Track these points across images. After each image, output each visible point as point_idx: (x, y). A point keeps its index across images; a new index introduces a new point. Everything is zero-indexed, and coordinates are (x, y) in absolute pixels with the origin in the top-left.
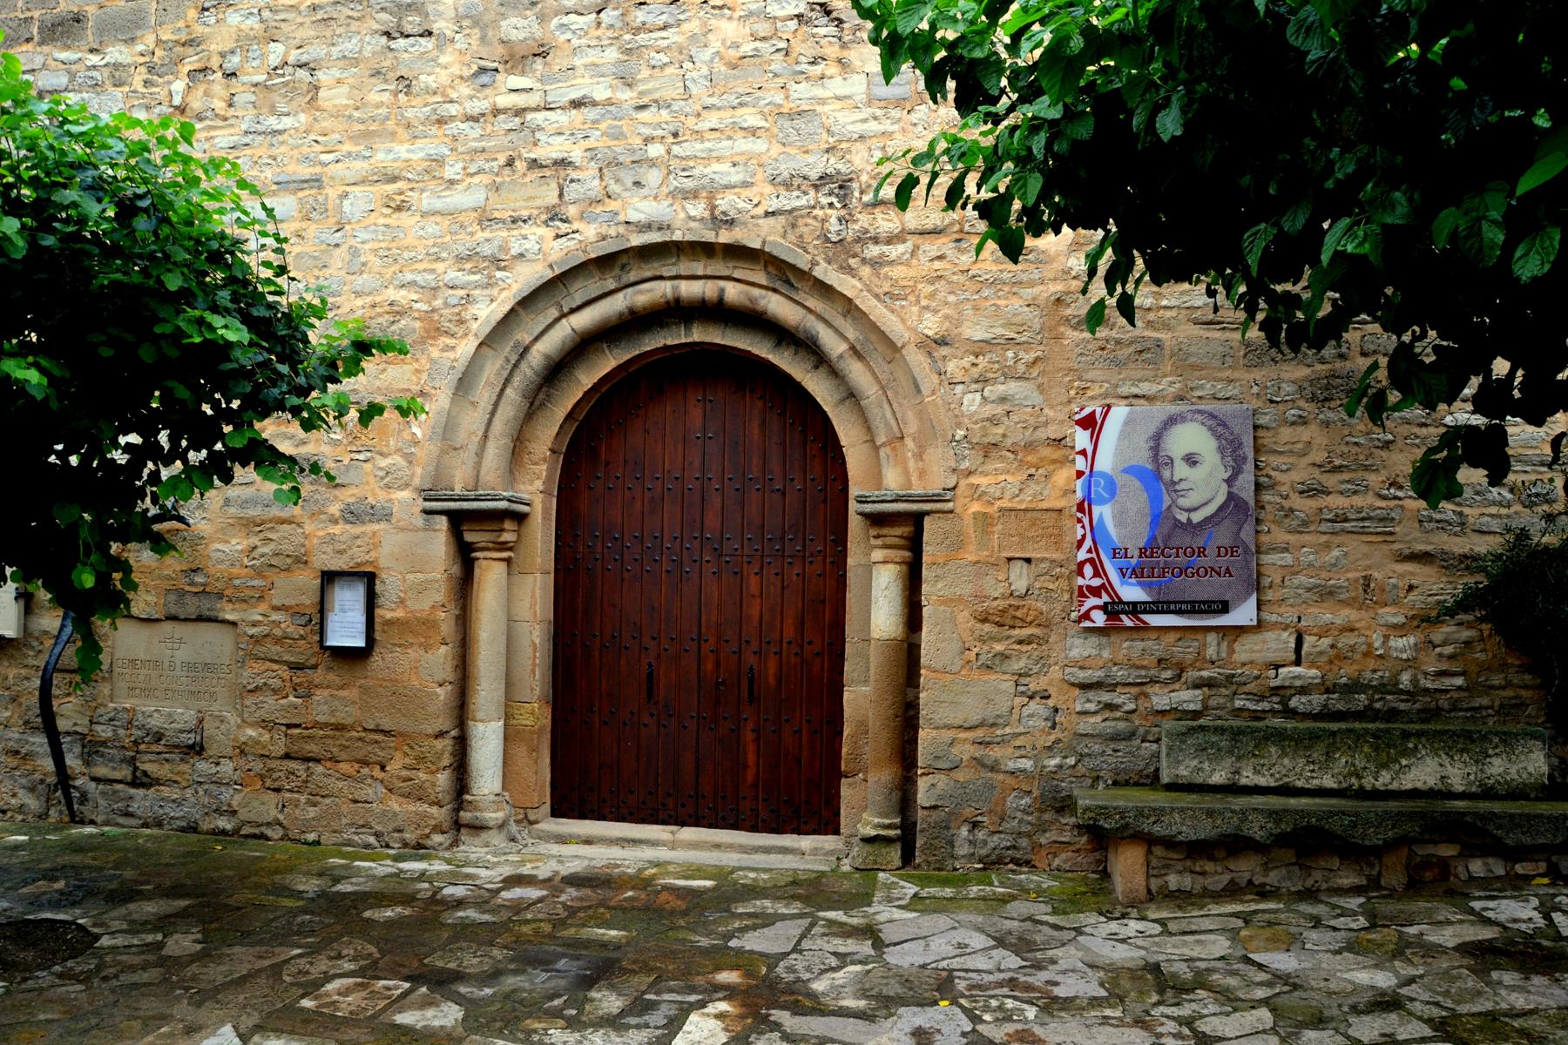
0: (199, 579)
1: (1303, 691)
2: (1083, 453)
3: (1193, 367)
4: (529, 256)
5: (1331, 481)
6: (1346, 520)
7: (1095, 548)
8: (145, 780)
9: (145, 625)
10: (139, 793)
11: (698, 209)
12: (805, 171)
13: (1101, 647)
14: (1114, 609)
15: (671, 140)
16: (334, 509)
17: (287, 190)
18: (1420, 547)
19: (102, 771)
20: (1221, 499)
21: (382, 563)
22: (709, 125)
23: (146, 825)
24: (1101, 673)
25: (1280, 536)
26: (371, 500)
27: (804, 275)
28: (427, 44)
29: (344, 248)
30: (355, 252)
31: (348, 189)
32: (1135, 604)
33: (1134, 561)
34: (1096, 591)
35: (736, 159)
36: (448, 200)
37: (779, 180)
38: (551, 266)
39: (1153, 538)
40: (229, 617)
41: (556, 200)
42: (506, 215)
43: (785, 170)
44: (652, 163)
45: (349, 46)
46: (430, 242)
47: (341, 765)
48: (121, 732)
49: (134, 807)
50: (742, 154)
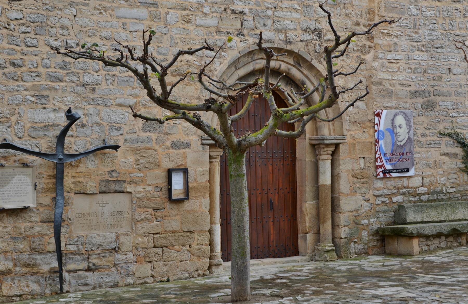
0: (115, 175)
1: (424, 194)
2: (377, 124)
3: (399, 98)
4: (233, 48)
5: (427, 132)
6: (431, 144)
7: (380, 154)
8: (93, 267)
9: (91, 196)
10: (90, 274)
12: (310, 27)
13: (126, 188)
14: (385, 172)
15: (274, 9)
16: (168, 143)
17: (144, 6)
18: (446, 151)
20: (406, 138)
21: (188, 165)
22: (285, 6)
23: (94, 288)
24: (381, 192)
26: (182, 140)
27: (305, 60)
29: (169, 35)
30: (172, 37)
31: (169, 10)
32: (389, 170)
33: (389, 157)
34: (380, 167)
35: (292, 20)
36: (205, 21)
37: (303, 29)
38: (239, 52)
39: (393, 150)
40: (129, 190)
41: (240, 27)
42: (225, 31)
43: (305, 25)
44: (268, 17)
46: (200, 38)
48: (81, 247)
49: (89, 281)
50: (294, 18)
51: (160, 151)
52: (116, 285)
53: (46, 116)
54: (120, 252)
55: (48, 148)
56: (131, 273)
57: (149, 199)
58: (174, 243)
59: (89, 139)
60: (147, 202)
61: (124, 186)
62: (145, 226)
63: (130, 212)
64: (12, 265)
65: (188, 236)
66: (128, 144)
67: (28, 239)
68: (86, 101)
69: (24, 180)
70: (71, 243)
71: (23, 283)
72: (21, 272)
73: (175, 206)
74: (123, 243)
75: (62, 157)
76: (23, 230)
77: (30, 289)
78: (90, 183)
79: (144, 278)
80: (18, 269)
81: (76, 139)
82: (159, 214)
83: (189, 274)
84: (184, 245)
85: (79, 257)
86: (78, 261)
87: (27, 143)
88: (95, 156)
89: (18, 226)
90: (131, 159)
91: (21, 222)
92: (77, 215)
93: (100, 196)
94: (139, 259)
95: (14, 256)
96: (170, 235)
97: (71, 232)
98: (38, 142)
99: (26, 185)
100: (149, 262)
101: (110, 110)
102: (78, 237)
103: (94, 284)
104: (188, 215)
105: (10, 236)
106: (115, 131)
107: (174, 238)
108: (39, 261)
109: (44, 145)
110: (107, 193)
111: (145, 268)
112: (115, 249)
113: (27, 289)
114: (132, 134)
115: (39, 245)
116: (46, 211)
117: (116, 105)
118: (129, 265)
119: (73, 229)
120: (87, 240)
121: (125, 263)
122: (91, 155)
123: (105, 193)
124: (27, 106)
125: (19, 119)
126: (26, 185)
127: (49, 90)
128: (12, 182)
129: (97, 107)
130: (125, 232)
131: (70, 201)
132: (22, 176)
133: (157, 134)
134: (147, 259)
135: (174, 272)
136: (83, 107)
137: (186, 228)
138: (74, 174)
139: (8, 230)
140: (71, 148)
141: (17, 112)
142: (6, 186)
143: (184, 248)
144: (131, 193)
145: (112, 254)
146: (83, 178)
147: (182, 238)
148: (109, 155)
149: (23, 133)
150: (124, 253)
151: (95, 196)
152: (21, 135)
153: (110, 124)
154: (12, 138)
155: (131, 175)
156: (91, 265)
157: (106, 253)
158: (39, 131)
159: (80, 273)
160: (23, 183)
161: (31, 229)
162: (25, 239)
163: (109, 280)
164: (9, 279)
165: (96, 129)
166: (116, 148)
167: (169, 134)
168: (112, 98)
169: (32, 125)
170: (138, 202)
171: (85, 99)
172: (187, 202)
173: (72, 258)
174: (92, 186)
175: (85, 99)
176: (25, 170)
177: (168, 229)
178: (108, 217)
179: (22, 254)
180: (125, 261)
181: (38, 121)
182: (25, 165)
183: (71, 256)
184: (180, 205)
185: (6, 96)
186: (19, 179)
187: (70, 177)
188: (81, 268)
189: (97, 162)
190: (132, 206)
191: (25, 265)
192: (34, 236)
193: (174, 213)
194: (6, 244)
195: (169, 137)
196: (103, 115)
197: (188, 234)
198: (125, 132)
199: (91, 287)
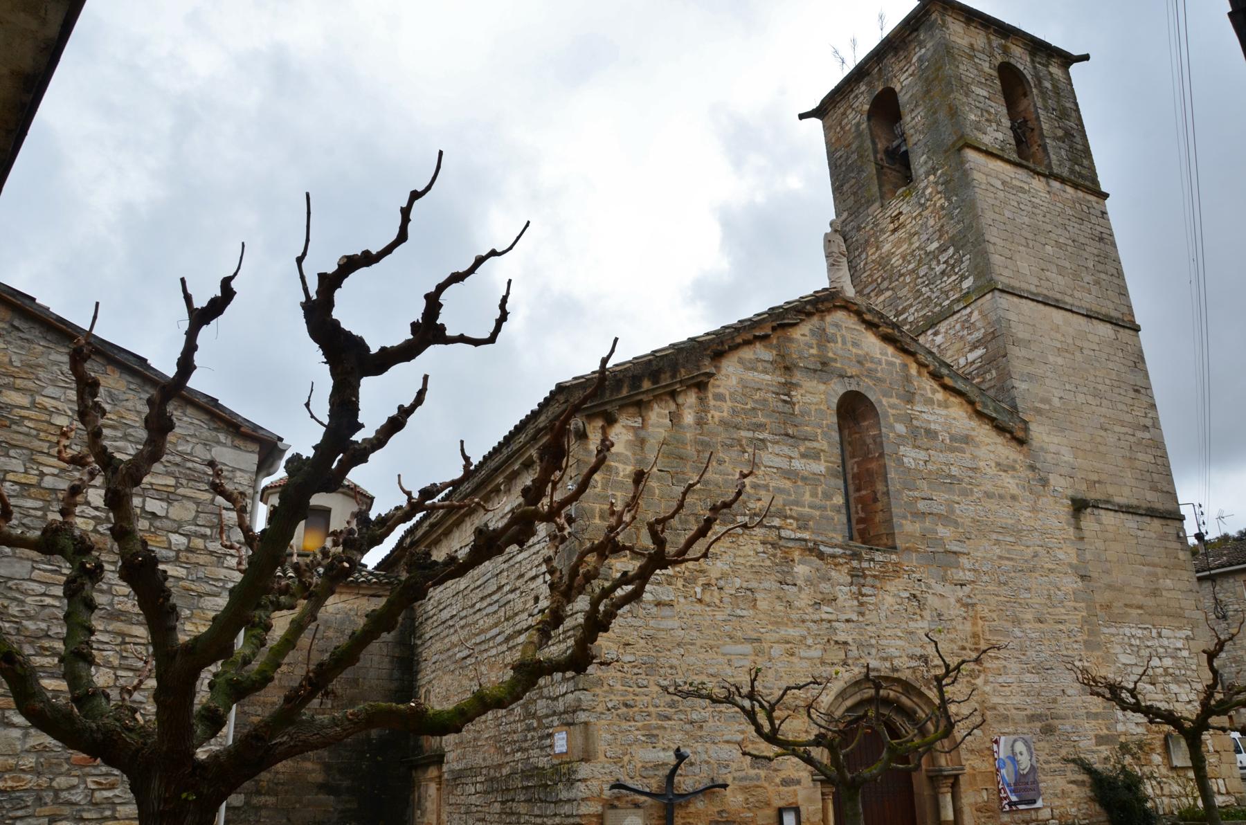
11: (888, 665)
16: (778, 780)
25: (1043, 777)
28: (795, 589)
45: (766, 585)
51: (770, 788)
90: (740, 798)
165: (705, 767)
185: (619, 736)
196: (710, 752)
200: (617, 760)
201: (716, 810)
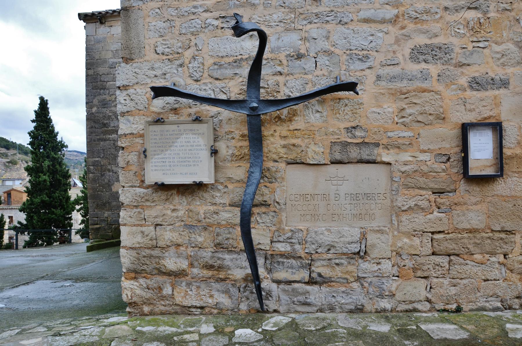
0: (358, 133)
8: (319, 279)
9: (312, 168)
10: (314, 288)
13: (380, 155)
16: (463, 81)
19: (282, 275)
21: (503, 118)
23: (321, 310)
26: (492, 74)
40: (385, 159)
47: (475, 256)
48: (297, 247)
49: (311, 299)
51: (448, 93)
52: (359, 310)
53: (238, 45)
54: (369, 258)
55: (240, 94)
56: (387, 294)
57: (424, 175)
58: (472, 249)
59: (310, 77)
60: (421, 179)
61: (376, 152)
62: (416, 219)
63: (388, 195)
64: (187, 264)
65: (501, 239)
66: (383, 83)
67: (211, 229)
68: (304, 19)
69: (194, 142)
70: (281, 239)
71: (205, 291)
72: (201, 275)
73: (476, 188)
74: (373, 246)
75: (255, 105)
76: (203, 216)
77: (215, 301)
78: (312, 147)
79: (412, 302)
80: (195, 271)
81: (288, 78)
82: (442, 200)
83: (502, 301)
84: (493, 254)
85: (294, 261)
86: (292, 267)
87: (207, 88)
88: (322, 102)
89: (195, 210)
90: (390, 107)
91: (198, 203)
92: (293, 197)
93: (333, 169)
94: (404, 272)
95: (190, 251)
96: (465, 235)
97: (280, 222)
98: (223, 85)
99: (197, 150)
100: (422, 278)
101: (348, 29)
102: (292, 231)
103: (320, 304)
104: (504, 203)
105: (183, 223)
106: (358, 62)
107: (472, 241)
108: (227, 263)
109: (235, 88)
110: (345, 163)
111: (415, 288)
112: (358, 253)
113: (210, 301)
114: (392, 67)
115: (227, 239)
116: (238, 190)
117: (358, 21)
118: (384, 281)
119: (284, 218)
120: (309, 236)
121: (378, 276)
122: (313, 101)
123: (340, 162)
124: (208, 33)
125: (196, 53)
126: (197, 150)
127: (243, 6)
128: (176, 144)
129: (324, 25)
130: (379, 227)
131: (279, 175)
132: (191, 136)
133: (440, 67)
134: (419, 273)
135: (472, 297)
136: (301, 27)
137: (497, 225)
138: (285, 133)
139: (180, 215)
140: (279, 92)
141: (192, 44)
142: (167, 150)
143: (493, 259)
144: (389, 164)
145: (353, 261)
146: (300, 140)
147: (489, 241)
148: (347, 101)
149: (201, 74)
150: (375, 261)
151: (323, 168)
152: (198, 76)
153: (348, 52)
154: (185, 81)
155: (390, 134)
156: (314, 275)
157: (342, 259)
158: (226, 68)
159: (296, 285)
160: (192, 146)
161: (214, 216)
162: (205, 229)
163: (347, 302)
164: (184, 284)
165: (323, 60)
166: (351, 87)
167: (464, 64)
168: (352, 10)
169: (217, 60)
170: (403, 180)
171: (304, 16)
172: (500, 181)
173: (283, 263)
174: (316, 151)
175: (304, 16)
176: (196, 126)
177: (461, 226)
178: (348, 202)
179: (201, 250)
180: (376, 274)
181: (225, 54)
182: (198, 120)
183: (280, 260)
184: (486, 185)
185: (178, 23)
186: (187, 140)
187: (278, 138)
188: (298, 280)
189: (325, 114)
190: (392, 185)
191: (206, 266)
192: (219, 225)
193: (474, 200)
194: (177, 234)
195: (464, 71)
196: (334, 37)
197: (503, 235)
198: (376, 64)
199: (316, 309)
200: (173, 57)
201: (343, 125)
